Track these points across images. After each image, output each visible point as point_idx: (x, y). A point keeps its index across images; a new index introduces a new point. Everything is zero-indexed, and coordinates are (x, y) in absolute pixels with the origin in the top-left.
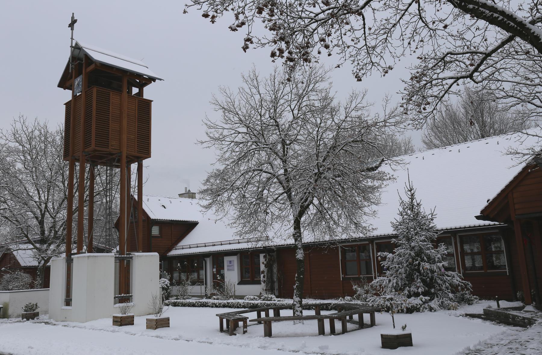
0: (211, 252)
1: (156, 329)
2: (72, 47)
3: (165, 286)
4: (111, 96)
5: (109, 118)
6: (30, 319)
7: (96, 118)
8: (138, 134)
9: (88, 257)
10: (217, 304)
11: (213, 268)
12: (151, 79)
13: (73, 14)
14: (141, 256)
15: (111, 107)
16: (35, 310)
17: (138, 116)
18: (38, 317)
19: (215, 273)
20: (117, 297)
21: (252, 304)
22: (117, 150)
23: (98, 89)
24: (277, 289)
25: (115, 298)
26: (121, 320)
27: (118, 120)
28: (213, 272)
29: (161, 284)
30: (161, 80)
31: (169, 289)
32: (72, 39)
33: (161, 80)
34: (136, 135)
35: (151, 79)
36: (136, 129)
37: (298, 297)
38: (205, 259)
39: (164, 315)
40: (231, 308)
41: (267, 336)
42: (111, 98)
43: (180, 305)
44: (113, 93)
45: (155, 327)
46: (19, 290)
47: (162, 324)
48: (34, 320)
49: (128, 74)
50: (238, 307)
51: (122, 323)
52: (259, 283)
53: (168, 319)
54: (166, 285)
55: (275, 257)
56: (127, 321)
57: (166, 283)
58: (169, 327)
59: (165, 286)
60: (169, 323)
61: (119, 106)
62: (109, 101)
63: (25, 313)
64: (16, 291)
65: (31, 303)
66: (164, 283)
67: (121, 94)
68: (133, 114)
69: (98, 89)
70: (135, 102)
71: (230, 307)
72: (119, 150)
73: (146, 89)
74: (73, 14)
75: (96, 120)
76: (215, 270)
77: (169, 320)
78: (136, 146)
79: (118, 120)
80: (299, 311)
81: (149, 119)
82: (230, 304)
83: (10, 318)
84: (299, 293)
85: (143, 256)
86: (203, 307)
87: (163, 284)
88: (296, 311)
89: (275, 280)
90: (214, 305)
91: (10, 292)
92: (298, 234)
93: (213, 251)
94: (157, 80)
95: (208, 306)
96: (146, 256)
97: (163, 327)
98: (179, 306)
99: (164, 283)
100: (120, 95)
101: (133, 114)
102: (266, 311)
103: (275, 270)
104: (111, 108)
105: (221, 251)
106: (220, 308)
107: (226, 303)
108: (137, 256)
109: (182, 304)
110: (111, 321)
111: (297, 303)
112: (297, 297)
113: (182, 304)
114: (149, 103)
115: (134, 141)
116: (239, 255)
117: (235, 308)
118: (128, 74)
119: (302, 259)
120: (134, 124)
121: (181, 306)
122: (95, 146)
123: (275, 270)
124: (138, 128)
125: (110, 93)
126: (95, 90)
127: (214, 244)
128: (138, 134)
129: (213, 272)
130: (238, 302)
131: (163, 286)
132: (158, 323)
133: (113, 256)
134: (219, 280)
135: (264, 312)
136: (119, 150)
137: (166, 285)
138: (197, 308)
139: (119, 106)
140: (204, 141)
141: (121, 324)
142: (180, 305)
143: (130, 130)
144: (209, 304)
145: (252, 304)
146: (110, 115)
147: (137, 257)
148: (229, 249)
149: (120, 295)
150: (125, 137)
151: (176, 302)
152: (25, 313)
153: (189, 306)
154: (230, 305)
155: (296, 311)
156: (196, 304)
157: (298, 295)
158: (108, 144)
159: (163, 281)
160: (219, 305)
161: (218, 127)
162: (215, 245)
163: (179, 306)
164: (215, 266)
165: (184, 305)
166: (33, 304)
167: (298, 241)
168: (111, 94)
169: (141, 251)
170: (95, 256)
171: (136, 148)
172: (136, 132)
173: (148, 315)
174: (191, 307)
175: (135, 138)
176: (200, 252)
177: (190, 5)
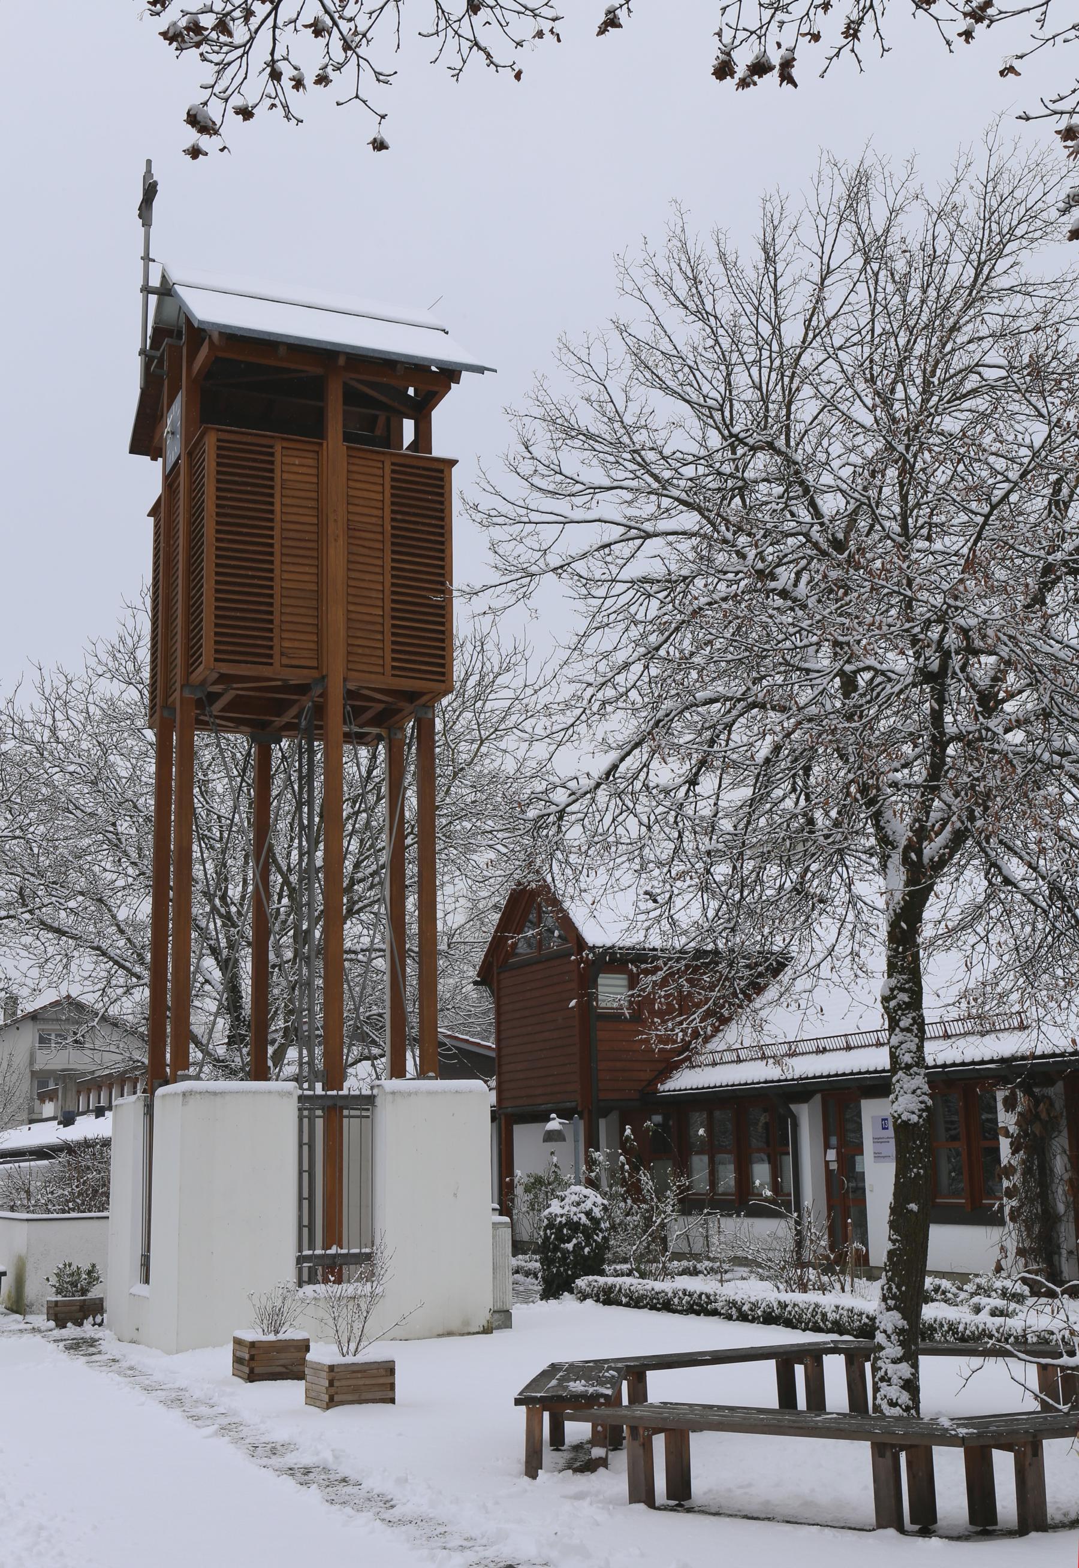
0: (807, 1078)
1: (328, 1408)
2: (146, 290)
3: (584, 1219)
4: (278, 458)
5: (271, 545)
6: (69, 1324)
7: (218, 548)
8: (393, 601)
9: (184, 1094)
10: (745, 1308)
11: (827, 1146)
12: (449, 374)
13: (149, 162)
14: (409, 1094)
15: (277, 500)
16: (88, 1291)
17: (393, 528)
18: (98, 1319)
19: (834, 1166)
20: (307, 1258)
21: (865, 1320)
22: (306, 671)
23: (226, 436)
24: (1070, 1253)
25: (300, 1260)
26: (252, 1358)
27: (309, 549)
28: (827, 1163)
29: (567, 1208)
30: (480, 370)
31: (601, 1230)
32: (147, 259)
33: (480, 370)
34: (388, 605)
35: (449, 374)
36: (388, 580)
37: (896, 1308)
38: (793, 1107)
39: (372, 1353)
40: (794, 1327)
41: (639, 1502)
42: (277, 467)
43: (624, 1300)
44: (285, 444)
45: (326, 1398)
46: (63, 1211)
47: (356, 1389)
48: (78, 1329)
49: (341, 361)
50: (817, 1329)
51: (257, 1370)
52: (997, 1220)
53: (389, 1369)
54: (588, 1214)
55: (1059, 1104)
56: (281, 1362)
57: (588, 1205)
58: (392, 1401)
59: (583, 1216)
60: (392, 1386)
61: (314, 495)
62: (272, 479)
63: (59, 1298)
64: (55, 1216)
65: (70, 1265)
66: (578, 1204)
67: (321, 444)
68: (374, 520)
69: (226, 436)
70: (380, 472)
71: (789, 1324)
72: (317, 668)
73: (440, 415)
74: (149, 162)
75: (217, 557)
76: (832, 1155)
77: (392, 1372)
78: (388, 646)
79: (309, 549)
80: (895, 1380)
81: (442, 535)
82: (789, 1308)
83: (31, 1313)
84: (898, 1287)
85: (416, 1093)
86: (698, 1313)
87: (574, 1209)
88: (882, 1379)
89: (1061, 1208)
90: (734, 1311)
91: (27, 1220)
92: (904, 997)
93: (814, 1077)
94: (465, 375)
95: (715, 1313)
96: (430, 1093)
97: (360, 1402)
98: (620, 1304)
99: (578, 1204)
100: (317, 452)
101: (374, 520)
102: (808, 1361)
103: (1060, 1164)
104: (277, 507)
105: (844, 1074)
106: (755, 1325)
107: (775, 1305)
108: (393, 1093)
109: (631, 1298)
110: (225, 1356)
111: (889, 1337)
112: (889, 1309)
113: (631, 1298)
114: (442, 471)
115: (379, 628)
116: (818, 1098)
117: (804, 1330)
118: (341, 361)
119: (914, 1118)
120: (379, 562)
121: (627, 1305)
122: (216, 660)
123: (1060, 1164)
124: (393, 576)
125: (271, 447)
126: (211, 442)
127: (822, 1044)
128: (393, 601)
129: (827, 1163)
130: (817, 1305)
131: (575, 1219)
132: (336, 1384)
133: (290, 1093)
134: (766, 1199)
135: (648, 1373)
136: (317, 668)
137: (588, 1214)
138: (677, 1317)
139: (314, 495)
140: (478, 587)
141: (252, 1371)
142: (624, 1300)
143: (362, 585)
144: (718, 1305)
145: (868, 1317)
146: (276, 533)
147: (390, 1097)
148: (871, 1069)
149: (310, 1252)
150: (336, 616)
151: (611, 1288)
152: (59, 1298)
153: (653, 1308)
154: (790, 1313)
155: (882, 1379)
156: (676, 1300)
157: (894, 1297)
158: (271, 648)
159: (575, 1198)
160: (751, 1310)
161: (535, 517)
162: (825, 1050)
163: (619, 1303)
164: (834, 1140)
165: (636, 1302)
166: (78, 1268)
167: (902, 1030)
168: (278, 448)
169: (431, 1074)
170: (215, 1094)
171: (388, 655)
172: (387, 592)
173: (439, 1336)
174: (659, 1310)
175: (383, 616)
176: (770, 1078)
177: (381, 5)
